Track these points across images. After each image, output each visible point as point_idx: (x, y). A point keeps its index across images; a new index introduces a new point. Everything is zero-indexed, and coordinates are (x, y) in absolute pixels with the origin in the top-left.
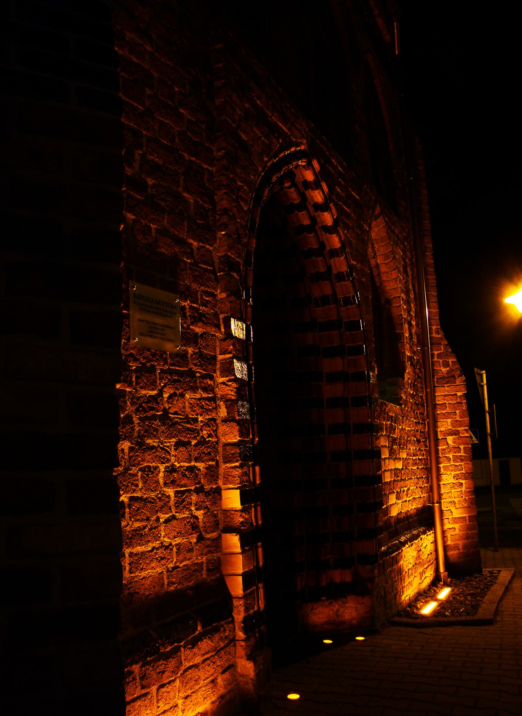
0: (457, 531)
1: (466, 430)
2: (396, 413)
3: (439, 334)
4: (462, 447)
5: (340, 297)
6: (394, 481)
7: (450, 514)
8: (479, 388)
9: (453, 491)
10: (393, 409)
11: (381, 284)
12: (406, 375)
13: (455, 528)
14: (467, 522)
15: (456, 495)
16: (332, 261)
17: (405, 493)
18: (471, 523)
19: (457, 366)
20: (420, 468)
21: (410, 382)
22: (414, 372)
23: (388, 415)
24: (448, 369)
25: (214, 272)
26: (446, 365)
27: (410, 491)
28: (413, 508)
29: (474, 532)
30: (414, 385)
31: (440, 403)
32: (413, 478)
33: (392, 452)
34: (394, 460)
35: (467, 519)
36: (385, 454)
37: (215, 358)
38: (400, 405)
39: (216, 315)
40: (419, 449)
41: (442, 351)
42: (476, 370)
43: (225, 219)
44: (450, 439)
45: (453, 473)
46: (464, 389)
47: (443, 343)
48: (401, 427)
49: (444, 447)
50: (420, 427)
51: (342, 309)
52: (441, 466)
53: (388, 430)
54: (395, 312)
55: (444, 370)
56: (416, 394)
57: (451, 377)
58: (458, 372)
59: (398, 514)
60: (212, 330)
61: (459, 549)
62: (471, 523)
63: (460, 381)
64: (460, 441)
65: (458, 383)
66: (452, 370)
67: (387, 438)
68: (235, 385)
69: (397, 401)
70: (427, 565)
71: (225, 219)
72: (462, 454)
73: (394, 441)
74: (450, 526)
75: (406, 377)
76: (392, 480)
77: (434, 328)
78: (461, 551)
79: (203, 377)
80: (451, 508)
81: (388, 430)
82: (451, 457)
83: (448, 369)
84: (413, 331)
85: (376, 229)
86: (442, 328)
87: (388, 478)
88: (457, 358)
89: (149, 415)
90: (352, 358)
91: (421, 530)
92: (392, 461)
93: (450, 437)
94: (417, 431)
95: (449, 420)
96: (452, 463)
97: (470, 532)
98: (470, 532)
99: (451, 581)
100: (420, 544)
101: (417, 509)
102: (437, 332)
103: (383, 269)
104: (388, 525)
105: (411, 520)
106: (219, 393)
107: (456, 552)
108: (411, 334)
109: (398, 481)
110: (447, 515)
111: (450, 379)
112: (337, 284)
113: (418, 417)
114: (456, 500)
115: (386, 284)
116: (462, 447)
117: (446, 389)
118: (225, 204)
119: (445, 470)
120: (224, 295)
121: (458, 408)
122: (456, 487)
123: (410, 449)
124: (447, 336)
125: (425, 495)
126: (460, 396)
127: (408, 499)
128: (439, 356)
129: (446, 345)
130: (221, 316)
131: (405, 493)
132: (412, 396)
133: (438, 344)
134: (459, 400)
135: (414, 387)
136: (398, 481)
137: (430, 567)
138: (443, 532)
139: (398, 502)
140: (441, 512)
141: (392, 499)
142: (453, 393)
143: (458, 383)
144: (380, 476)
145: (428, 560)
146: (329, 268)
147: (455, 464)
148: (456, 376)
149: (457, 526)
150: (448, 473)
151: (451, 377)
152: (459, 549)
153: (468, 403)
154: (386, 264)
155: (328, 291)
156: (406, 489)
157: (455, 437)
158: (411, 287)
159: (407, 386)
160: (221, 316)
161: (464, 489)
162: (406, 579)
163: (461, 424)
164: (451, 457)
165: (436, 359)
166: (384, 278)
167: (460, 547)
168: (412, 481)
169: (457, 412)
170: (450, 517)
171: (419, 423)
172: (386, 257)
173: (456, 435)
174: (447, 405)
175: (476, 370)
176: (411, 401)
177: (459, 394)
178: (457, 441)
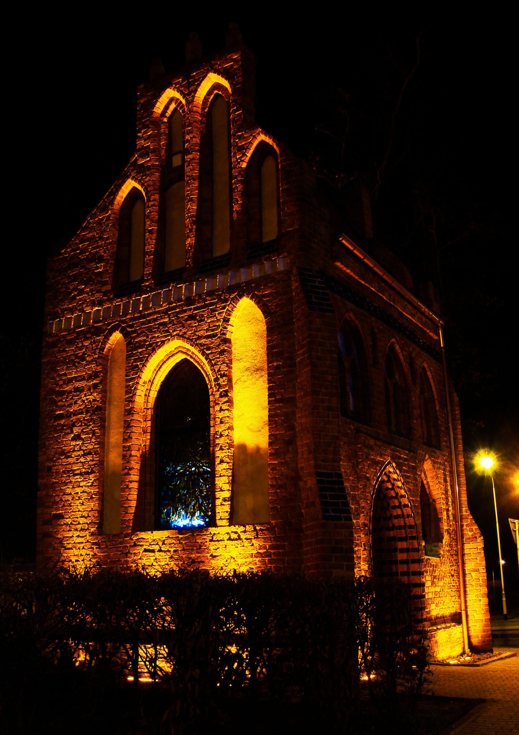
0: (477, 628)
1: (483, 569)
2: (436, 563)
3: (467, 512)
4: (481, 578)
5: (405, 514)
6: (435, 597)
7: (473, 617)
8: (513, 532)
9: (475, 604)
10: (434, 560)
11: (430, 492)
12: (444, 540)
13: (476, 626)
14: (484, 623)
15: (477, 607)
16: (401, 499)
17: (442, 604)
18: (486, 623)
19: (478, 531)
20: (453, 590)
21: (446, 543)
22: (450, 537)
23: (431, 564)
24: (472, 533)
25: (360, 529)
26: (472, 530)
27: (445, 603)
28: (448, 612)
29: (488, 628)
30: (450, 545)
31: (467, 553)
32: (448, 596)
33: (433, 583)
34: (435, 587)
35: (484, 620)
36: (428, 584)
37: (361, 557)
38: (440, 557)
39: (361, 543)
40: (453, 580)
41: (469, 523)
42: (510, 520)
43: (363, 510)
44: (473, 574)
45: (475, 594)
46: (482, 545)
47: (469, 518)
48: (439, 570)
49: (469, 579)
50: (453, 568)
51: (406, 519)
52: (467, 589)
53: (431, 572)
54: (438, 506)
55: (470, 534)
56: (452, 549)
57: (475, 537)
58: (479, 535)
59: (437, 615)
60: (360, 548)
61: (478, 638)
62: (486, 623)
63: (480, 539)
64: (479, 575)
65: (478, 541)
66: (475, 534)
67: (430, 576)
68: (367, 565)
69: (438, 555)
70: (456, 644)
71: (363, 510)
72: (481, 582)
73: (435, 577)
74: (474, 624)
75: (444, 541)
76: (433, 597)
77: (464, 509)
78: (480, 639)
79: (358, 564)
80: (474, 614)
81: (431, 572)
82: (474, 585)
83: (472, 533)
84: (450, 513)
85: (427, 465)
86: (469, 509)
87: (430, 596)
88: (478, 526)
89: (162, 515)
90: (411, 541)
91: (453, 624)
92: (433, 587)
93: (473, 573)
94: (452, 570)
95: (473, 563)
96: (475, 588)
97: (485, 628)
98: (485, 628)
99: (471, 655)
100: (451, 632)
101: (451, 613)
102: (466, 512)
103: (431, 484)
104: (429, 619)
105: (446, 618)
106: (362, 568)
107: (477, 639)
108: (448, 516)
109: (437, 597)
110: (470, 618)
111: (474, 538)
112: (404, 509)
113: (452, 562)
114: (477, 609)
115: (432, 491)
116: (481, 578)
117: (471, 544)
118: (363, 505)
119: (470, 592)
120: (363, 536)
121: (479, 556)
122: (477, 602)
123: (446, 580)
124: (472, 513)
125: (457, 606)
126: (480, 549)
127: (444, 607)
128: (467, 525)
129: (472, 519)
130: (363, 543)
131: (442, 604)
132: (449, 551)
133: (466, 518)
134: (479, 551)
135: (449, 546)
136: (437, 597)
137: (458, 645)
138: (468, 628)
139: (436, 608)
140: (467, 616)
141: (433, 606)
142: (475, 547)
143: (478, 541)
144: (425, 595)
145: (457, 641)
146: (400, 503)
147: (477, 588)
148: (478, 537)
149: (477, 624)
150: (472, 593)
151: (475, 537)
152: (478, 638)
153: (485, 553)
154: (433, 482)
155: (400, 512)
156: (442, 602)
157: (476, 572)
158: (449, 488)
159: (444, 547)
160: (363, 543)
161: (482, 603)
162: (440, 647)
163: (480, 565)
164: (474, 585)
165: (465, 527)
166: (431, 488)
167: (480, 637)
168: (447, 598)
169: (478, 558)
170: (473, 619)
171: (453, 565)
172: (433, 478)
173: (477, 571)
174: (472, 554)
175: (510, 520)
176: (447, 554)
177: (479, 547)
178: (478, 575)
